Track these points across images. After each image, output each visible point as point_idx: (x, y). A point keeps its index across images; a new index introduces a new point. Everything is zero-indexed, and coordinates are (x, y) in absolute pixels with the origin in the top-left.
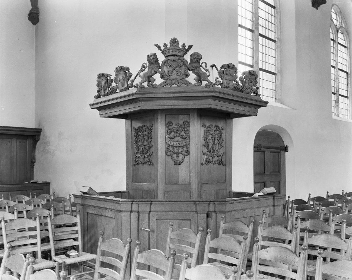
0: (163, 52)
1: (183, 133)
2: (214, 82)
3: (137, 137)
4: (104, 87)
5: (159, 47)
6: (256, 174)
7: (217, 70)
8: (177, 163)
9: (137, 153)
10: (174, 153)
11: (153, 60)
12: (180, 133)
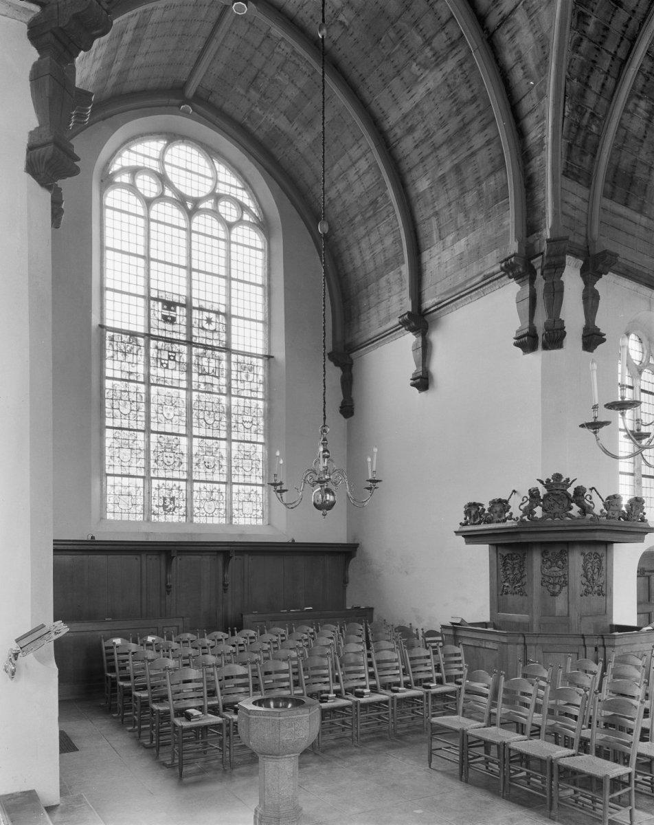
0: (546, 487)
1: (560, 563)
2: (599, 514)
3: (505, 565)
4: (474, 515)
5: (542, 482)
6: (639, 603)
7: (603, 501)
8: (554, 595)
9: (504, 582)
10: (551, 584)
11: (534, 494)
12: (557, 563)
